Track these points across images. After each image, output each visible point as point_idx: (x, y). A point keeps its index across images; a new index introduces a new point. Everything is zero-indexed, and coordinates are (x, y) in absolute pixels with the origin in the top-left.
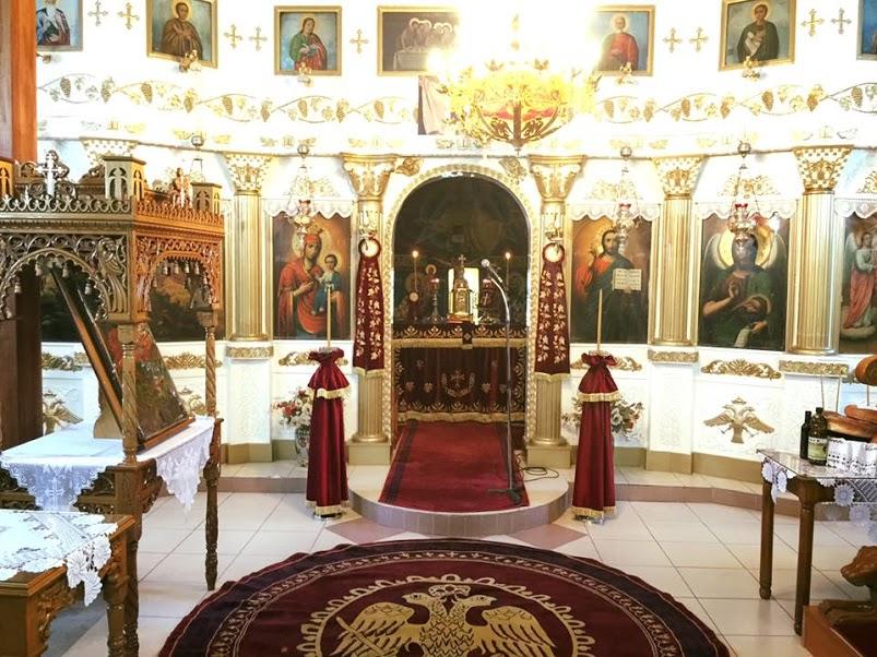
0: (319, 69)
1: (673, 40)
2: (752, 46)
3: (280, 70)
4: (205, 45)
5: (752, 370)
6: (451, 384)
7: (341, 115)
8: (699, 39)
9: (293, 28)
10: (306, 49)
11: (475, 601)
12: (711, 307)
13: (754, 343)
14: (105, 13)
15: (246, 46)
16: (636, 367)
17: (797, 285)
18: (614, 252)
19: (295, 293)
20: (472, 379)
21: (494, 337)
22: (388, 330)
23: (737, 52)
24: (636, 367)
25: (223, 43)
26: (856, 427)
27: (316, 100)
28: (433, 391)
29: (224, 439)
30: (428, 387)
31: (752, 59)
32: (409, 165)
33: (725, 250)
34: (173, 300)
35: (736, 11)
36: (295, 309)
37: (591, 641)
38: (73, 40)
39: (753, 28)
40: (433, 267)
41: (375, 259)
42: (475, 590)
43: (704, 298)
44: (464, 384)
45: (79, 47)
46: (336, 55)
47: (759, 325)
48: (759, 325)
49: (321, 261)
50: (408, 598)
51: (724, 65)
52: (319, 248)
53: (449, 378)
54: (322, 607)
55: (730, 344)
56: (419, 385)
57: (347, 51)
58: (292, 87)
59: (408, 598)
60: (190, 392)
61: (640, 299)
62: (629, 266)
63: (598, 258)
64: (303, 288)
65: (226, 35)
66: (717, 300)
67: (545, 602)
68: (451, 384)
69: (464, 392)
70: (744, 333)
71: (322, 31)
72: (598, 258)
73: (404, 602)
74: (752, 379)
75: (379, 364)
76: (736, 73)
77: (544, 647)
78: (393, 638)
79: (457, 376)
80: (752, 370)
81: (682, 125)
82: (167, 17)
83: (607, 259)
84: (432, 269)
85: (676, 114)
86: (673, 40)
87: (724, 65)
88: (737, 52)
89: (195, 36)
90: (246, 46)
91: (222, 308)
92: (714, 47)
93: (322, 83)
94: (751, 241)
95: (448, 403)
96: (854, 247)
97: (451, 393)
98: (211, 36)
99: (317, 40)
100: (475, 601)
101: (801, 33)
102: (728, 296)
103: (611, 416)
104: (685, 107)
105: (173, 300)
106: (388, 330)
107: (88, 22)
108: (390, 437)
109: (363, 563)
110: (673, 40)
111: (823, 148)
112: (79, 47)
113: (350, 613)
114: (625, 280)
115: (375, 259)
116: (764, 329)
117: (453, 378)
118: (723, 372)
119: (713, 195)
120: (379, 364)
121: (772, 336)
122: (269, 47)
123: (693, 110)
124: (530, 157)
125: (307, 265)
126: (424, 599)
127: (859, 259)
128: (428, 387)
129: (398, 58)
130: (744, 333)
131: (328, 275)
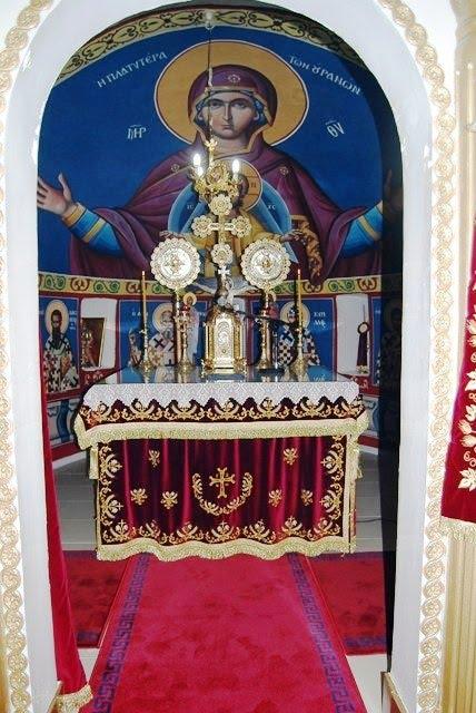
6: (211, 494)
17: (460, 564)
20: (248, 485)
21: (342, 482)
26: (150, 193)
28: (178, 508)
29: (385, 656)
30: (169, 499)
40: (194, 297)
53: (205, 481)
68: (211, 494)
69: (234, 505)
79: (222, 479)
84: (191, 298)
91: (376, 545)
95: (206, 524)
97: (210, 508)
103: (307, 490)
108: (445, 583)
117: (214, 481)
128: (169, 499)
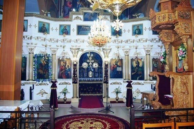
0: (67, 34)
1: (125, 31)
2: (137, 32)
3: (60, 34)
4: (48, 31)
5: (139, 84)
7: (70, 42)
8: (129, 31)
9: (63, 28)
10: (64, 31)
11: (92, 121)
12: (133, 73)
13: (140, 79)
14: (31, 26)
15: (54, 31)
16: (121, 84)
18: (117, 64)
19: (62, 72)
22: (78, 77)
23: (134, 33)
24: (121, 84)
25: (51, 30)
27: (66, 39)
30: (85, 89)
31: (137, 34)
32: (82, 50)
33: (135, 65)
34: (40, 73)
35: (134, 27)
36: (62, 75)
37: (110, 125)
38: (26, 30)
39: (137, 29)
41: (76, 64)
42: (92, 120)
43: (132, 72)
44: (91, 89)
45: (27, 31)
46: (70, 32)
47: (140, 76)
48: (140, 76)
49: (66, 66)
50: (80, 121)
51: (133, 35)
52: (66, 64)
54: (66, 122)
55: (136, 80)
56: (83, 89)
57: (71, 31)
58: (61, 37)
59: (80, 121)
60: (43, 90)
61: (121, 72)
62: (119, 67)
63: (114, 65)
64: (63, 71)
65: (37, 26)
66: (134, 72)
67: (104, 121)
68: (89, 89)
70: (138, 78)
71: (67, 28)
72: (114, 65)
73: (80, 122)
74: (140, 85)
75: (76, 83)
76: (134, 36)
77: (102, 127)
78: (77, 126)
80: (139, 84)
81: (127, 44)
82: (42, 26)
83: (116, 66)
85: (126, 42)
86: (125, 31)
87: (133, 35)
88: (134, 33)
89: (46, 29)
90: (54, 31)
92: (131, 32)
93: (67, 37)
94: (138, 63)
96: (154, 63)
97: (89, 90)
98: (49, 29)
99: (66, 30)
100: (92, 121)
101: (144, 30)
102: (135, 71)
104: (127, 41)
105: (40, 73)
106: (78, 77)
107: (28, 27)
109: (73, 116)
110: (129, 31)
111: (148, 48)
112: (27, 31)
113: (70, 123)
114: (119, 69)
115: (76, 64)
116: (141, 77)
118: (135, 84)
119: (132, 55)
120: (76, 83)
121: (142, 78)
122: (58, 31)
123: (128, 42)
124: (103, 49)
125: (64, 67)
126: (83, 121)
127: (155, 66)
128: (85, 89)
129: (80, 32)
130: (138, 78)
131: (68, 69)
